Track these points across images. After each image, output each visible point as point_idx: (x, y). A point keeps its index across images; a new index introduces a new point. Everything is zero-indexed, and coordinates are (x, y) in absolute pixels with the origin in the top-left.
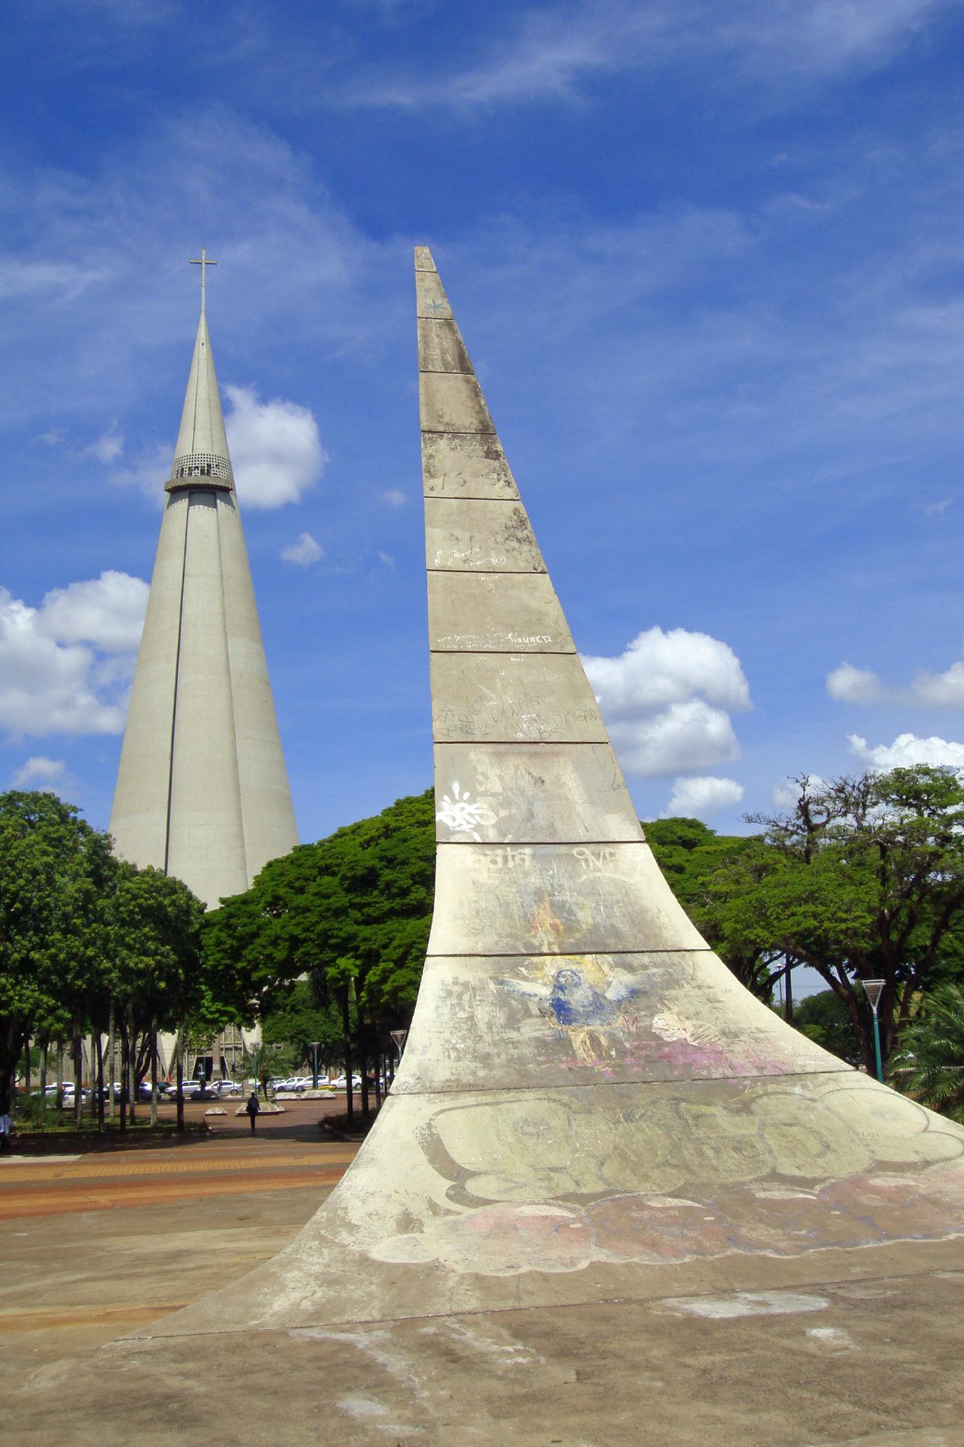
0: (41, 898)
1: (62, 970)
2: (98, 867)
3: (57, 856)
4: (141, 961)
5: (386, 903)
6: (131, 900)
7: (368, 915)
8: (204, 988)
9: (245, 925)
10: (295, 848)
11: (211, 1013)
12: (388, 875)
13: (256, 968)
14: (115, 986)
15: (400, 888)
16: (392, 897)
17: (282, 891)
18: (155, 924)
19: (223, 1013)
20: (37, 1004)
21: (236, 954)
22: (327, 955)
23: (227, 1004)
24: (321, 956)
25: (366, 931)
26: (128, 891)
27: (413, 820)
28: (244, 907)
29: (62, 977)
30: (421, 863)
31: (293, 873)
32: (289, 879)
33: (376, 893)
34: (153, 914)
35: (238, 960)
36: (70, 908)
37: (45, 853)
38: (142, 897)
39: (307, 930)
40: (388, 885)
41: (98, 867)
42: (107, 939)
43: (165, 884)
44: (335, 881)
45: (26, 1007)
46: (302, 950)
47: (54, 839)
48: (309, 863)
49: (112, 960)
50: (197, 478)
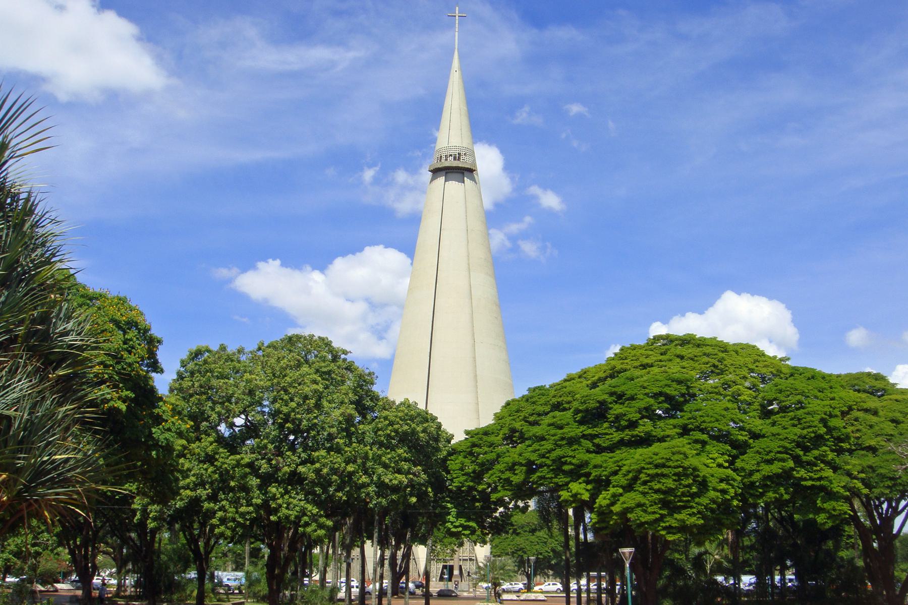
0: (308, 420)
1: (325, 483)
2: (361, 398)
3: (326, 387)
4: (395, 479)
5: (615, 434)
6: (388, 425)
7: (598, 446)
8: (449, 505)
9: (486, 453)
10: (529, 390)
11: (456, 527)
12: (617, 409)
13: (495, 490)
14: (371, 499)
15: (629, 420)
16: (620, 429)
17: (517, 425)
18: (409, 448)
19: (465, 528)
20: (303, 512)
21: (477, 477)
22: (561, 479)
23: (469, 520)
24: (555, 480)
25: (597, 459)
26: (386, 418)
27: (637, 364)
28: (485, 438)
29: (325, 491)
30: (648, 399)
31: (529, 409)
32: (519, 421)
33: (606, 425)
34: (407, 439)
35: (479, 483)
36: (334, 430)
37: (315, 382)
38: (398, 423)
39: (543, 456)
40: (618, 418)
41: (361, 398)
42: (366, 457)
43: (419, 414)
44: (569, 414)
45: (293, 514)
46: (538, 474)
47: (324, 373)
48: (542, 401)
49: (370, 476)
50: (451, 162)
